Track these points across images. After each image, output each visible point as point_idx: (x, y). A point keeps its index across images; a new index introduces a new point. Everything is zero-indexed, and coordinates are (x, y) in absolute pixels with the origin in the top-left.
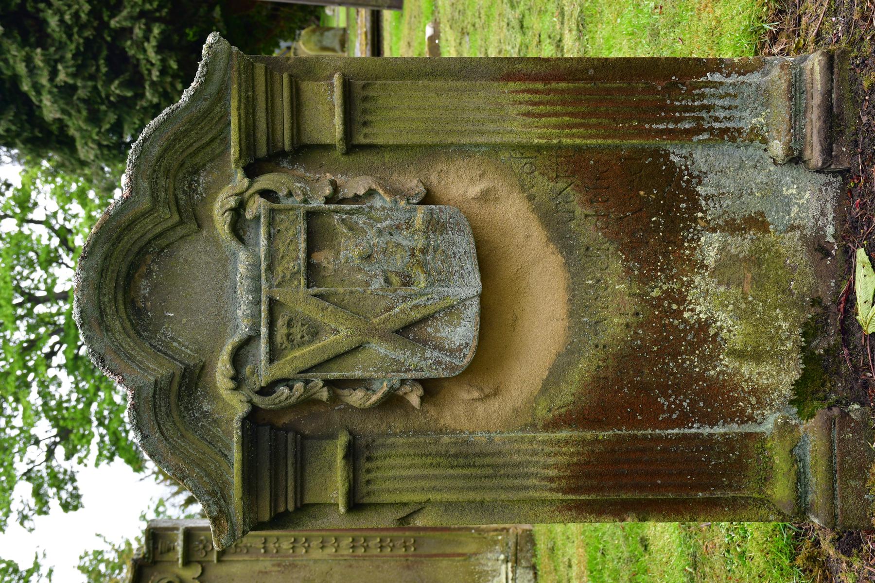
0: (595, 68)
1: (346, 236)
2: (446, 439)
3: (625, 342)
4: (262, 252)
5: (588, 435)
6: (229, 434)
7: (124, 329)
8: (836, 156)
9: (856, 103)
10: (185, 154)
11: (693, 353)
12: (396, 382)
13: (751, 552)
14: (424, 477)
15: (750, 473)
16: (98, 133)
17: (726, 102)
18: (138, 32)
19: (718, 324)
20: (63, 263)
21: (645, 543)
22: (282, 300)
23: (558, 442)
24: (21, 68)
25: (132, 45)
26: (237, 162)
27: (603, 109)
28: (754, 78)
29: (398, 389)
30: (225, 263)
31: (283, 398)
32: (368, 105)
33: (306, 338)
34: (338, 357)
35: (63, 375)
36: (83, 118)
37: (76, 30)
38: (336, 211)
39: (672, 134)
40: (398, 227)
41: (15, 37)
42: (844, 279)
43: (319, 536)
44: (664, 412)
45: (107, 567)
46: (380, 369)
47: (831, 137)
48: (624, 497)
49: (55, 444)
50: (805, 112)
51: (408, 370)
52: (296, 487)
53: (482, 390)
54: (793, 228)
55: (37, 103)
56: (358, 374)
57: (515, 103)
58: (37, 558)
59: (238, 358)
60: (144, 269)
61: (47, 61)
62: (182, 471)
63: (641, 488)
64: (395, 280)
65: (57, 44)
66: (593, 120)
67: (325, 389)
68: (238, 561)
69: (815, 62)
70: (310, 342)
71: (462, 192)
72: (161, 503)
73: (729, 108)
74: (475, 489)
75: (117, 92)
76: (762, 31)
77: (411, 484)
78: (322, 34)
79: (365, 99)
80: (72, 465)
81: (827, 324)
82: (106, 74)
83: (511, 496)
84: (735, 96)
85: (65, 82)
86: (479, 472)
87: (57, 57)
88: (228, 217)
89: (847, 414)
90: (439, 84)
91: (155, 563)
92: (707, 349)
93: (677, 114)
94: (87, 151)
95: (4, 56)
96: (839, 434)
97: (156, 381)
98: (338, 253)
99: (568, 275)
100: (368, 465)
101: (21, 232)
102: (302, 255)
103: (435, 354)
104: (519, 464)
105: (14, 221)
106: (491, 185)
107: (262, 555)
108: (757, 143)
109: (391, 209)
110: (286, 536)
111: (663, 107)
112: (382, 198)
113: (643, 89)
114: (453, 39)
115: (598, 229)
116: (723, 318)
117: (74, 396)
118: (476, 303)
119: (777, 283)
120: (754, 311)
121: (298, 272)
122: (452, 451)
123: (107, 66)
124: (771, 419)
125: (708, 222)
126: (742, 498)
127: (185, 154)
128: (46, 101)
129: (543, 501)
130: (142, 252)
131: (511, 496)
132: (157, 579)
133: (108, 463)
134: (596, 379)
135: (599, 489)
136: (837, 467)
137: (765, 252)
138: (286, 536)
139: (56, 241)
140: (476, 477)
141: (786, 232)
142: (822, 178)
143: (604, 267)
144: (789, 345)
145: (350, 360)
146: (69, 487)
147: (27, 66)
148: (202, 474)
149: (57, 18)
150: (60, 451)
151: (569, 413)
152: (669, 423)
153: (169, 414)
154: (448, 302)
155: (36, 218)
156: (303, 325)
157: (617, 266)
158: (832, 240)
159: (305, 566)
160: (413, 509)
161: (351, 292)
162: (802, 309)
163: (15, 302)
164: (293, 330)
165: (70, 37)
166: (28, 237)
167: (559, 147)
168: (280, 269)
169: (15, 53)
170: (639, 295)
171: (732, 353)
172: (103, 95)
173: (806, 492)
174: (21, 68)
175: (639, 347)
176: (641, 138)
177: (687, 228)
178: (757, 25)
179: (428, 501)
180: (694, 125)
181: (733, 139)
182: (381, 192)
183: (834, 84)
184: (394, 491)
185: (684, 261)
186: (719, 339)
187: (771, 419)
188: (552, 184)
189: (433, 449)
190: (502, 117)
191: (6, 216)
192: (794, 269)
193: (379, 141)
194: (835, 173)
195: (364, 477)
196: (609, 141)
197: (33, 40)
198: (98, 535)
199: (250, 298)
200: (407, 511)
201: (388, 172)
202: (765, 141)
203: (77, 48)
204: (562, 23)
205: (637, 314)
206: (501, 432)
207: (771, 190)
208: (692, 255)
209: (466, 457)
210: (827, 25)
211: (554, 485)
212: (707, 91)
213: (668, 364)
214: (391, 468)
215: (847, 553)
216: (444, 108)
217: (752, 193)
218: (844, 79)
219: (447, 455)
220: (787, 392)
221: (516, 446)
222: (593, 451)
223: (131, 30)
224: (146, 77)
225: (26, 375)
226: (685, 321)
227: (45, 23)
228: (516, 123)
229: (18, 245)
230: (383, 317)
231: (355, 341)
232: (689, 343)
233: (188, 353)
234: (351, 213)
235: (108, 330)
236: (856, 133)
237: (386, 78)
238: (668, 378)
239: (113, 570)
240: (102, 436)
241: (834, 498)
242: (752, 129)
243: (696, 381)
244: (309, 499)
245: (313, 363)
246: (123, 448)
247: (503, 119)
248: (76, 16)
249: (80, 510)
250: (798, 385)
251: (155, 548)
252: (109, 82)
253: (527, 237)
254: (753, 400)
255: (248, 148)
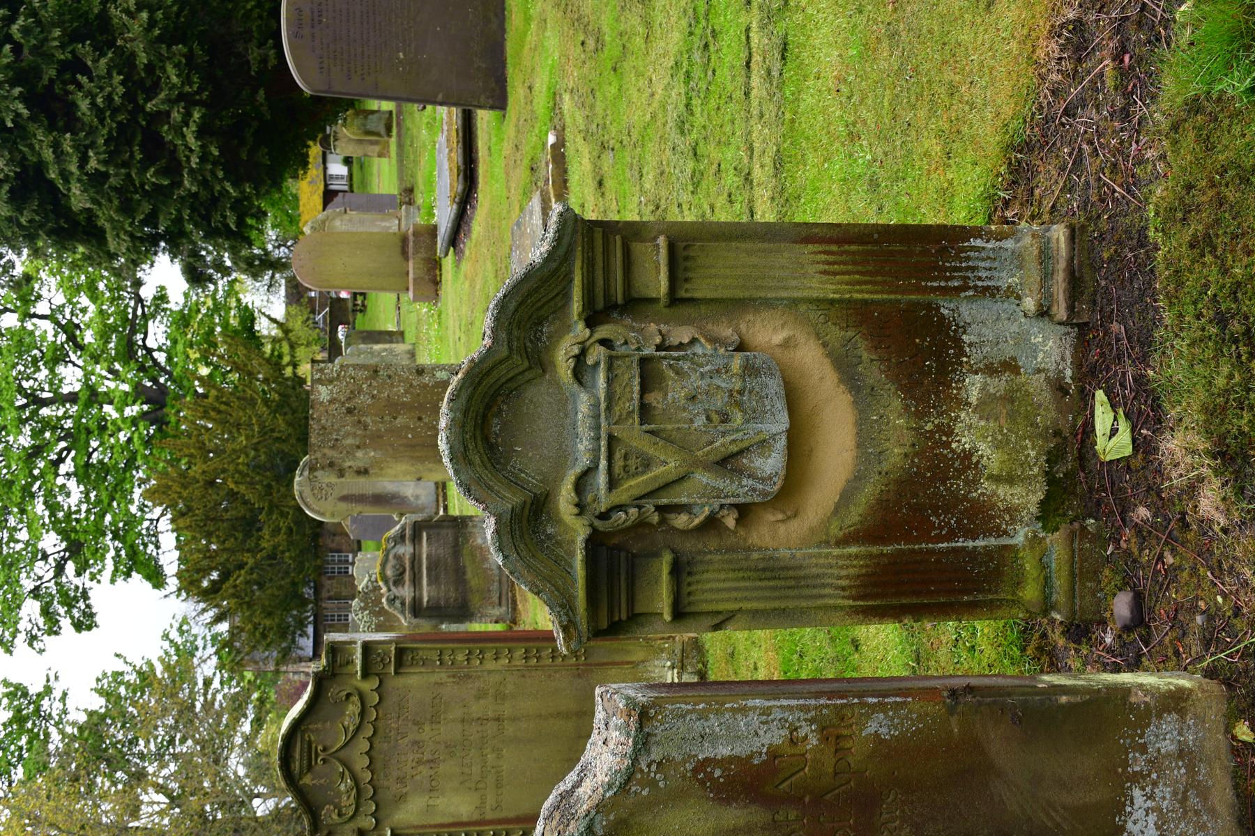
0: (879, 233)
1: (673, 379)
2: (755, 555)
3: (904, 469)
4: (602, 395)
5: (875, 549)
6: (572, 554)
7: (482, 462)
8: (1078, 312)
9: (1095, 269)
10: (534, 307)
11: (959, 478)
12: (717, 507)
13: (980, 645)
14: (736, 589)
15: (1005, 579)
16: (131, 224)
17: (987, 264)
18: (176, 116)
19: (980, 453)
20: (70, 361)
21: (856, 644)
22: (620, 436)
23: (849, 556)
24: (48, 154)
25: (169, 130)
26: (579, 315)
27: (887, 269)
28: (1009, 244)
29: (717, 513)
30: (565, 405)
31: (621, 521)
32: (688, 264)
33: (640, 469)
34: (667, 485)
35: (72, 484)
36: (114, 207)
37: (108, 113)
38: (665, 358)
39: (944, 291)
40: (718, 371)
41: (41, 121)
42: (1079, 414)
43: (493, 648)
44: (935, 529)
45: (127, 690)
46: (703, 496)
47: (1074, 296)
48: (904, 602)
49: (65, 560)
50: (1052, 274)
51: (726, 496)
52: (628, 600)
53: (784, 512)
54: (1039, 371)
55: (65, 192)
56: (684, 500)
57: (813, 262)
58: (48, 680)
59: (581, 484)
60: (495, 409)
61: (75, 147)
62: (537, 587)
63: (917, 594)
64: (715, 417)
65: (87, 129)
66: (879, 278)
67: (656, 513)
68: (414, 673)
69: (1059, 233)
70: (643, 473)
71: (767, 339)
72: (185, 621)
73: (990, 269)
74: (780, 598)
75: (154, 180)
76: (996, 197)
77: (726, 595)
78: (366, 118)
79: (687, 258)
80: (84, 581)
81: (1066, 453)
82: (140, 161)
83: (810, 604)
84: (995, 259)
85: (96, 169)
86: (783, 583)
87: (87, 142)
88: (572, 362)
89: (1086, 528)
90: (749, 245)
91: (334, 675)
92: (971, 474)
93: (948, 274)
94: (118, 243)
95: (29, 142)
96: (1079, 544)
97: (513, 508)
98: (666, 394)
99: (856, 412)
100: (689, 579)
101: (24, 328)
102: (636, 396)
103: (750, 482)
104: (818, 576)
105: (16, 316)
106: (791, 333)
107: (438, 667)
108: (1012, 299)
109: (712, 356)
110: (461, 648)
111: (936, 268)
112: (702, 345)
113: (920, 252)
114: (587, 151)
115: (881, 372)
116: (984, 448)
117: (84, 507)
118: (784, 437)
119: (1026, 417)
120: (1008, 442)
121: (633, 412)
122: (761, 565)
123: (141, 152)
124: (1022, 533)
125: (971, 366)
126: (998, 600)
127: (534, 307)
128: (76, 189)
129: (836, 608)
130: (496, 394)
131: (810, 604)
132: (337, 691)
133: (125, 580)
134: (879, 501)
135: (882, 596)
136: (1077, 571)
137: (1017, 391)
138: (461, 648)
139: (62, 337)
140: (781, 588)
141: (1034, 374)
142: (1063, 329)
143: (886, 404)
144: (1036, 470)
145: (677, 488)
146: (82, 605)
147: (54, 152)
148: (553, 588)
149: (88, 101)
150: (70, 567)
151: (857, 531)
152: (940, 539)
153: (522, 537)
154: (762, 437)
155: (39, 312)
156: (637, 458)
157: (897, 403)
158: (1070, 381)
159: (479, 677)
160: (727, 616)
161: (679, 429)
162: (1046, 439)
163: (18, 404)
164: (629, 462)
165: (102, 121)
166: (32, 333)
167: (849, 301)
168: (617, 409)
169: (42, 138)
170: (915, 429)
171: (991, 477)
172: (137, 183)
173: (1051, 593)
174: (48, 154)
175: (915, 473)
176: (919, 293)
177: (954, 371)
178: (992, 191)
179: (740, 610)
180: (961, 283)
181: (993, 296)
182: (702, 340)
183: (1076, 252)
184: (712, 601)
185: (952, 399)
186: (980, 466)
187: (1022, 533)
188: (843, 333)
189: (744, 564)
190: (803, 274)
191: (6, 310)
192: (1040, 406)
193: (698, 295)
194: (1072, 326)
195: (686, 590)
196: (892, 297)
197: (61, 124)
198: (117, 655)
199: (592, 434)
200: (721, 618)
201: (704, 322)
202: (1019, 298)
203: (110, 132)
204: (751, 157)
205: (914, 445)
206: (801, 549)
207: (1021, 339)
208: (958, 394)
209: (772, 571)
210: (1062, 199)
211: (847, 593)
212: (972, 254)
213: (939, 488)
214: (709, 581)
215: (1078, 642)
216: (754, 266)
217: (1007, 341)
218: (1083, 248)
219: (756, 570)
220: (1034, 509)
221: (814, 560)
222: (879, 564)
223: (168, 114)
224: (184, 164)
225: (32, 485)
226: (953, 451)
227: (74, 105)
228: (814, 280)
229: (20, 341)
230: (705, 450)
231: (682, 471)
232: (956, 470)
233: (534, 482)
234: (678, 359)
235: (470, 463)
236: (1095, 293)
237: (701, 240)
238: (939, 499)
239: (134, 692)
240: (117, 550)
241: (1074, 597)
242: (1009, 287)
243: (962, 502)
244: (639, 609)
245: (646, 491)
246: (142, 563)
247: (804, 275)
248: (109, 98)
249: (95, 628)
250: (1042, 503)
251: (334, 661)
252: (143, 169)
253: (822, 378)
254: (1007, 517)
255: (589, 302)
